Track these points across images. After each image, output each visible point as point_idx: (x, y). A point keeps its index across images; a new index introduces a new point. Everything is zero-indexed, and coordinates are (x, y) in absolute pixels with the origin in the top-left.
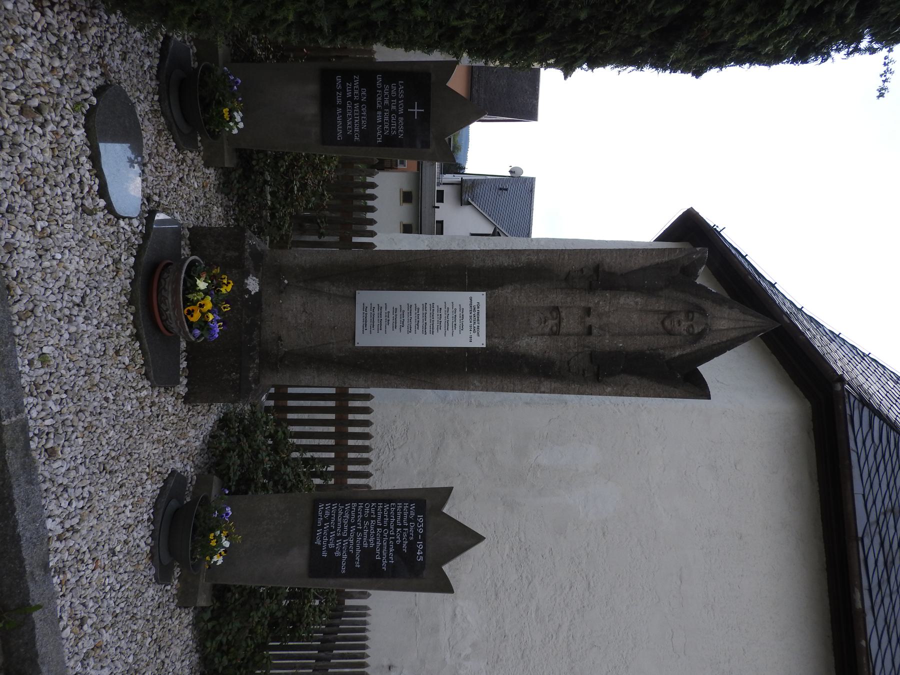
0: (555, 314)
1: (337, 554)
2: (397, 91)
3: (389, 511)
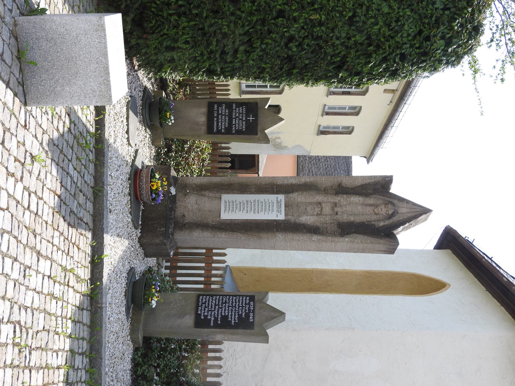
0: (319, 206)
1: (209, 317)
2: (242, 110)
3: (236, 300)
